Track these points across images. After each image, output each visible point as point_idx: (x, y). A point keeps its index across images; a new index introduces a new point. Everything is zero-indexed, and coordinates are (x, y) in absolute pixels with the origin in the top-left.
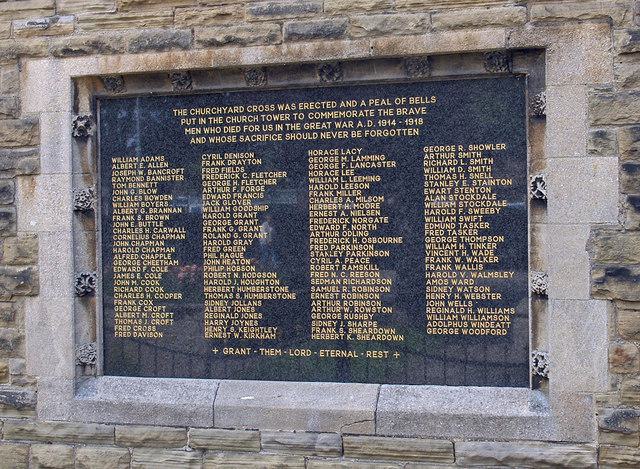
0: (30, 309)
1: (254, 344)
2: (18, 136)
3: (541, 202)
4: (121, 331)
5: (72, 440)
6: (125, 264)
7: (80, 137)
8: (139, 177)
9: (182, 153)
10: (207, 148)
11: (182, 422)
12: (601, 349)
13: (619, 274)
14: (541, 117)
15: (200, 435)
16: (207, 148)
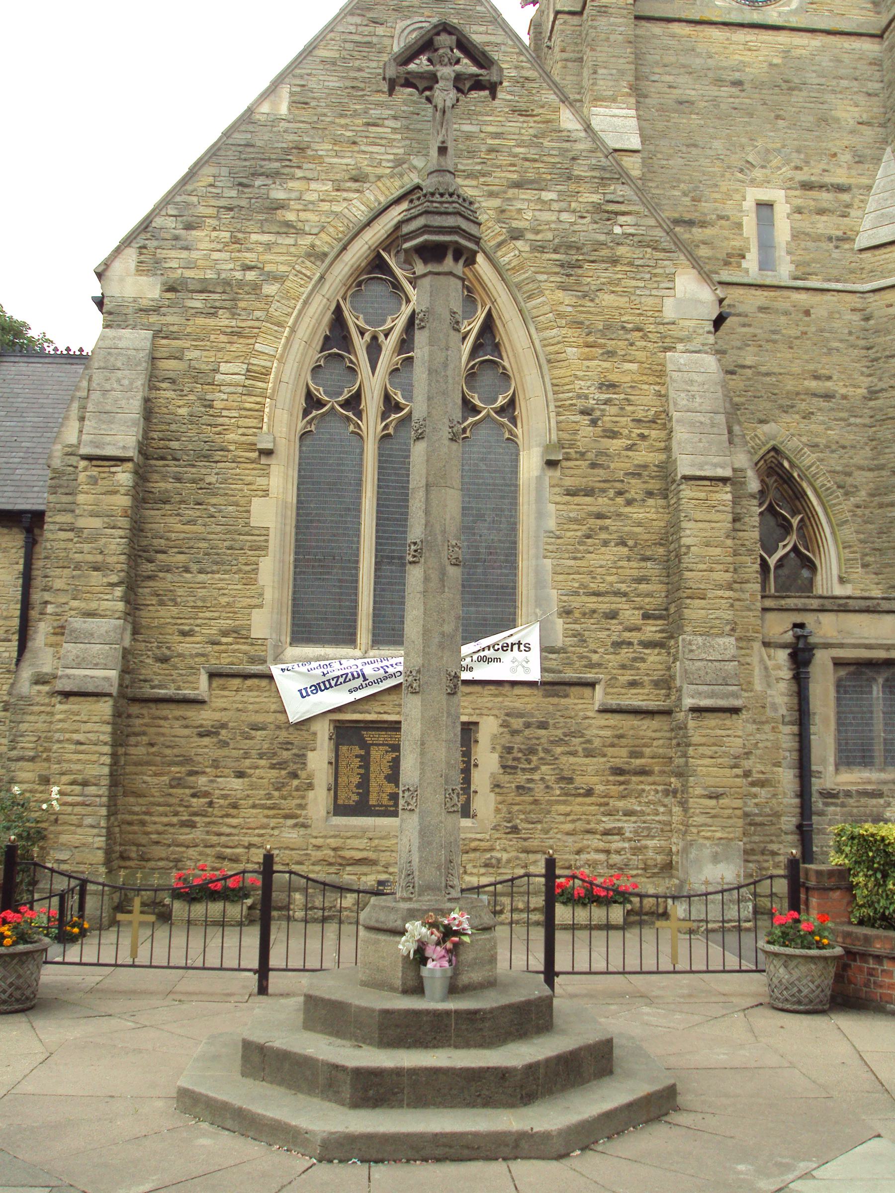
0: (311, 794)
1: (386, 806)
2: (310, 737)
3: (476, 765)
4: (340, 802)
5: (325, 837)
6: (343, 780)
7: (330, 739)
8: (351, 752)
9: (366, 746)
10: (373, 744)
11: (364, 830)
12: (492, 806)
13: (498, 786)
14: (477, 741)
15: (370, 835)
16: (373, 744)
